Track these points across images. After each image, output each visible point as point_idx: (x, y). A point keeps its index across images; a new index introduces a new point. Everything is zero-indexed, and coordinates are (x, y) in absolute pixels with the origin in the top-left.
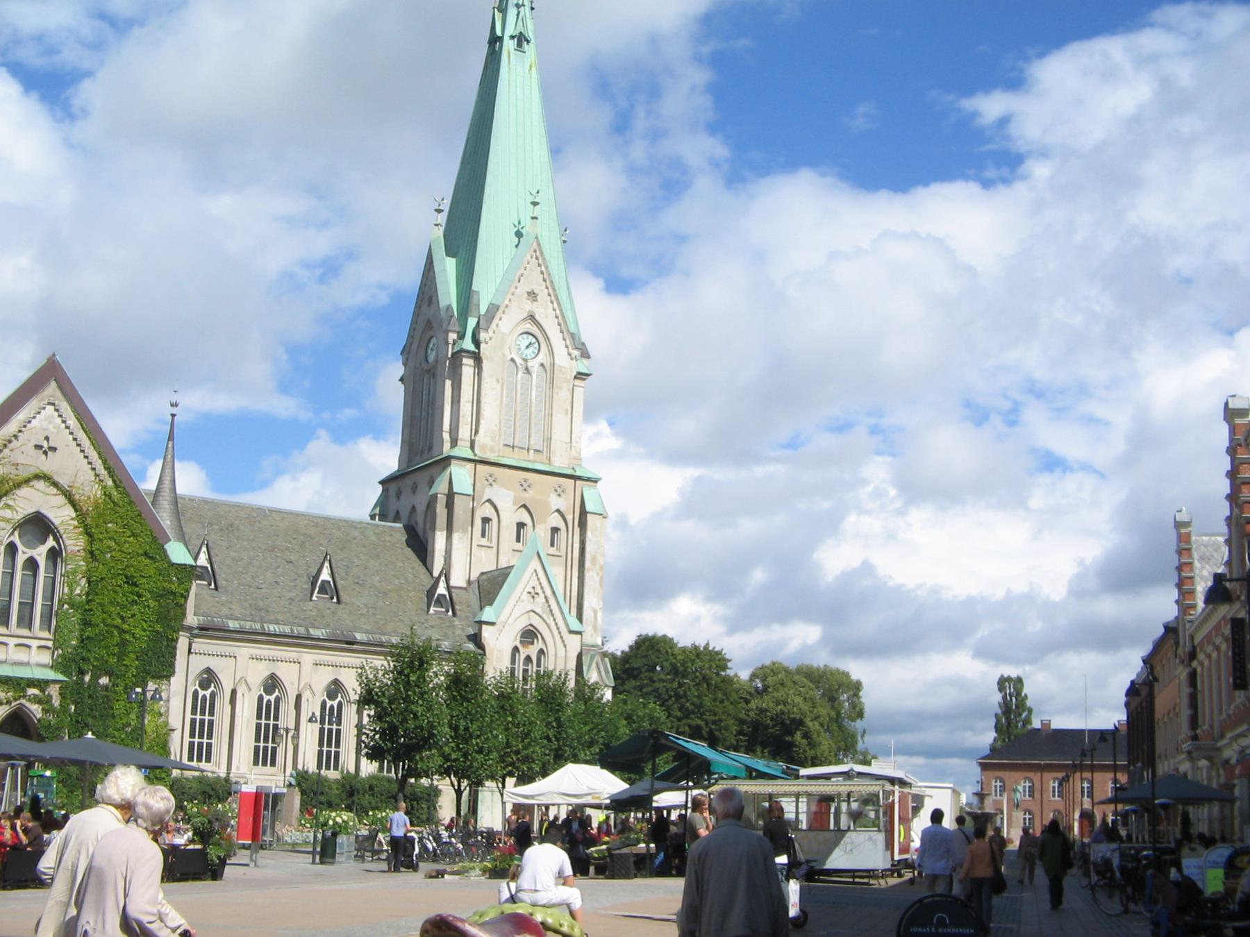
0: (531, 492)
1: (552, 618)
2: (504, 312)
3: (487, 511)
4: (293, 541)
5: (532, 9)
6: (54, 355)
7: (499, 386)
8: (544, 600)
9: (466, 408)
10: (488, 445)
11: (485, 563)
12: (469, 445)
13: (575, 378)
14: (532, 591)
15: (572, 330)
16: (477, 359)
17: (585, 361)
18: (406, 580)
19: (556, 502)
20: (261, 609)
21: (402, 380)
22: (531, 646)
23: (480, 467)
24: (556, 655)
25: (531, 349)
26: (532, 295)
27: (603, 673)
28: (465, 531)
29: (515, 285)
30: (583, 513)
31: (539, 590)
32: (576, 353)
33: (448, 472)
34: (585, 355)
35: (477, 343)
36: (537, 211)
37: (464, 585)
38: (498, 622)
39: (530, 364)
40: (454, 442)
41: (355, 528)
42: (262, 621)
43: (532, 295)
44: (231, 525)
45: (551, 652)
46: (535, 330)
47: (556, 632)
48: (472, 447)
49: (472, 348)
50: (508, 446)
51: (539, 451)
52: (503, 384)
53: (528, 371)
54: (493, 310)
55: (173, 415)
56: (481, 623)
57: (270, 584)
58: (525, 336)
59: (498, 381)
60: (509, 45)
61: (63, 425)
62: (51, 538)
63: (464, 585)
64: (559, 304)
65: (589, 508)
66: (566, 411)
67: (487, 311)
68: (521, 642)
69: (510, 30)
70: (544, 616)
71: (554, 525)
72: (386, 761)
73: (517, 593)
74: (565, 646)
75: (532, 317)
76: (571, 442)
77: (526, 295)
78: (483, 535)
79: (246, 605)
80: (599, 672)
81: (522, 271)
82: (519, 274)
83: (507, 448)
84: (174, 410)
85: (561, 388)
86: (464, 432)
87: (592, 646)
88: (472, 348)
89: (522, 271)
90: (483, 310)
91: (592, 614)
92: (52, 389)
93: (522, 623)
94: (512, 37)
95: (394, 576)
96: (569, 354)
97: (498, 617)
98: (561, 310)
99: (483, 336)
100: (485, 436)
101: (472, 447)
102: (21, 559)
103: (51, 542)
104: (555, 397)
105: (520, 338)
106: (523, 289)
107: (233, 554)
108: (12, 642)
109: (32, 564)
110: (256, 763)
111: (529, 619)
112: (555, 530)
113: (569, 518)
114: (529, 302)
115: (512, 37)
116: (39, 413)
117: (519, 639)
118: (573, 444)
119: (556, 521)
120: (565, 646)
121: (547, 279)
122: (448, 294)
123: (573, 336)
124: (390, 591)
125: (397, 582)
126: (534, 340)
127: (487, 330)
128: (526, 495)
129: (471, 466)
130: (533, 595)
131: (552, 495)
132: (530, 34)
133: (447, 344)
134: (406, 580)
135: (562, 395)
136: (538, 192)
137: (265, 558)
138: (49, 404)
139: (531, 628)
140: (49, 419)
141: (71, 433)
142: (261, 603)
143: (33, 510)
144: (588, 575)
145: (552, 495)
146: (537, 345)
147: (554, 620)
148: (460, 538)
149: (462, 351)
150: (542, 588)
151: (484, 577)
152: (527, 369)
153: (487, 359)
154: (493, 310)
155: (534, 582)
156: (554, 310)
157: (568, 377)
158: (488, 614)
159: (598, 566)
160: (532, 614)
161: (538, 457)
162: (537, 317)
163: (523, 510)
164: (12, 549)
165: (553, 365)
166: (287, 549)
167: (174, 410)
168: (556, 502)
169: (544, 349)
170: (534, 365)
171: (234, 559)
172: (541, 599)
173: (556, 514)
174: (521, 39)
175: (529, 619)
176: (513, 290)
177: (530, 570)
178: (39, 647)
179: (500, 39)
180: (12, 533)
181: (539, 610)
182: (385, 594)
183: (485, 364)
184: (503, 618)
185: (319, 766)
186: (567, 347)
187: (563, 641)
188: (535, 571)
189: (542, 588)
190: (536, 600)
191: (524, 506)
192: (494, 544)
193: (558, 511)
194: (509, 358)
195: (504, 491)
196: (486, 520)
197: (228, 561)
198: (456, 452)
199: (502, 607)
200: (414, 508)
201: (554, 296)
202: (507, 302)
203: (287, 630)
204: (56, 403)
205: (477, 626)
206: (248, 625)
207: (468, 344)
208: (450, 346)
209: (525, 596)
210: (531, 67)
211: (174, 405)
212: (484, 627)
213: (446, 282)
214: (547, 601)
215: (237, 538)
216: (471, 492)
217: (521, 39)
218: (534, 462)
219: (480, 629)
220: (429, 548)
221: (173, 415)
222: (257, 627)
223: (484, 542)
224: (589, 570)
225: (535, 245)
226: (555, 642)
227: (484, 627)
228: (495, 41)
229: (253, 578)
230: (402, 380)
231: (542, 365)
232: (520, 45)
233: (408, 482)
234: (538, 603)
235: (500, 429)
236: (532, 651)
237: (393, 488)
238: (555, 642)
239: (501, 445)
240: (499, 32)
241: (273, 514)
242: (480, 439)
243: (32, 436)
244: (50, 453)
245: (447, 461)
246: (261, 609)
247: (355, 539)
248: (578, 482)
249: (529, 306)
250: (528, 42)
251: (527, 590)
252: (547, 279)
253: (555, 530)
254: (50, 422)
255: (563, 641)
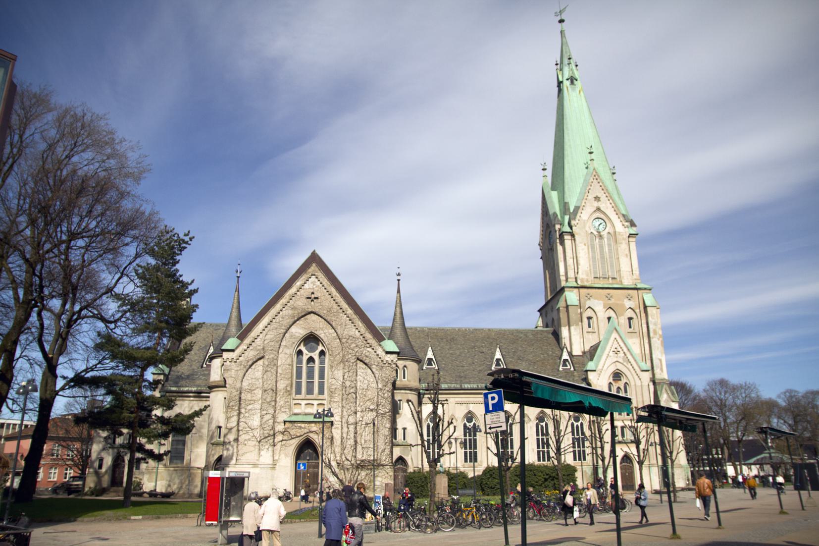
0: (613, 301)
1: (629, 364)
2: (583, 209)
3: (589, 313)
4: (486, 343)
5: (577, 66)
6: (314, 251)
7: (586, 247)
8: (623, 355)
9: (570, 261)
10: (585, 277)
11: (591, 341)
12: (574, 280)
13: (629, 237)
14: (615, 350)
15: (624, 213)
16: (572, 235)
17: (634, 228)
18: (548, 355)
19: (628, 304)
20: (462, 377)
21: (541, 258)
22: (619, 382)
23: (581, 290)
24: (635, 385)
25: (601, 226)
26: (597, 199)
27: (670, 394)
28: (577, 325)
29: (586, 195)
30: (645, 307)
31: (619, 349)
32: (628, 224)
33: (564, 295)
34: (633, 224)
35: (571, 228)
36: (593, 156)
37: (581, 354)
38: (597, 369)
39: (602, 233)
40: (567, 280)
41: (522, 333)
42: (461, 383)
43: (597, 199)
44: (453, 339)
45: (632, 383)
46: (602, 216)
47: (633, 372)
48: (576, 281)
49: (568, 230)
50: (597, 278)
51: (614, 278)
52: (588, 246)
53: (601, 237)
54: (577, 209)
55: (399, 280)
56: (587, 371)
57: (469, 364)
58: (597, 220)
59: (585, 245)
60: (566, 83)
61: (321, 285)
62: (321, 345)
63: (581, 354)
64: (613, 200)
65: (647, 304)
66: (627, 255)
67: (574, 210)
68: (614, 380)
69: (566, 76)
70: (625, 363)
71: (629, 316)
72: (124, 485)
73: (606, 352)
74: (640, 379)
75: (598, 209)
76: (632, 271)
77: (594, 199)
78: (589, 327)
79: (454, 375)
80: (668, 394)
81: (590, 187)
82: (588, 189)
83: (596, 279)
84: (399, 278)
85: (621, 243)
86: (571, 274)
87: (662, 380)
88: (568, 230)
89: (590, 187)
90: (572, 211)
91: (659, 362)
92: (314, 268)
93: (612, 369)
94: (568, 79)
95: (541, 353)
96: (623, 225)
97: (597, 367)
98: (615, 203)
99: (573, 223)
100: (582, 274)
101: (576, 281)
102: (305, 358)
103: (320, 348)
104: (619, 248)
105: (594, 221)
106: (591, 197)
107: (451, 352)
108: (303, 402)
109: (311, 360)
110: (466, 461)
111: (616, 366)
112: (630, 319)
113: (637, 311)
114: (596, 202)
115: (568, 79)
116: (308, 280)
117: (611, 378)
118: (634, 272)
119: (630, 313)
120: (640, 379)
121: (604, 189)
122: (555, 207)
123: (624, 215)
124: (538, 361)
125: (542, 356)
126: (602, 221)
127: (574, 219)
128: (610, 302)
129: (576, 290)
130: (617, 353)
131: (625, 300)
132: (577, 76)
133: (556, 231)
134: (548, 355)
135: (623, 247)
136: (591, 147)
137: (469, 352)
138: (312, 275)
139: (619, 371)
140: (313, 283)
141: (325, 289)
142: (462, 374)
143: (309, 332)
144: (653, 341)
145: (625, 300)
146: (604, 224)
147: (631, 365)
148: (575, 329)
149: (563, 232)
150: (621, 348)
151: (592, 348)
152: (601, 236)
153: (577, 234)
154: (577, 209)
155: (617, 346)
156: (611, 204)
157: (625, 237)
158: (590, 365)
159: (658, 335)
160: (617, 363)
161: (614, 281)
162: (602, 209)
163: (610, 310)
164: (300, 353)
165: (615, 232)
166: (482, 346)
167: (399, 278)
168: (628, 304)
169: (609, 225)
170: (604, 233)
171: (451, 354)
172: (621, 354)
173: (630, 310)
174: (572, 80)
175: (616, 366)
176: (585, 197)
177: (612, 338)
178: (318, 405)
179: (562, 82)
180: (299, 345)
181: (621, 361)
182: (535, 363)
183: (577, 237)
184: (600, 367)
185: (539, 460)
186: (621, 221)
187: (639, 377)
188: (615, 339)
189: (621, 348)
190: (619, 355)
191: (610, 308)
192: (596, 330)
193: (630, 308)
194: (590, 232)
195: (596, 301)
196: (589, 318)
197: (448, 356)
198: (568, 284)
199: (599, 361)
200: (553, 319)
201: (610, 197)
202: (583, 204)
203: (475, 386)
204: (316, 274)
205: (585, 373)
206: (453, 386)
207: (567, 229)
208: (557, 232)
209: (611, 354)
210: (580, 91)
211: (399, 275)
212: (589, 373)
213: (552, 202)
214: (625, 355)
215: (455, 344)
216: (577, 303)
217: (572, 80)
218: (612, 284)
219: (587, 375)
220: (560, 334)
221: (399, 280)
222: (458, 386)
223: (590, 330)
224: (653, 338)
225: (594, 173)
226: (634, 378)
227: (589, 373)
228: (560, 83)
229: (460, 362)
230: (541, 258)
231: (609, 233)
232: (572, 83)
233: (549, 306)
234: (620, 357)
235: (590, 270)
236: (621, 384)
237: (544, 311)
238: (634, 378)
239: (593, 277)
240: (561, 79)
241: (477, 331)
242: (580, 276)
243: (305, 292)
244: (315, 300)
245: (562, 290)
246: (462, 377)
247: (520, 338)
248: (639, 291)
249: (596, 204)
250: (577, 80)
251: (612, 350)
252: (604, 189)
253: (630, 319)
254: (314, 285)
255: (639, 377)
